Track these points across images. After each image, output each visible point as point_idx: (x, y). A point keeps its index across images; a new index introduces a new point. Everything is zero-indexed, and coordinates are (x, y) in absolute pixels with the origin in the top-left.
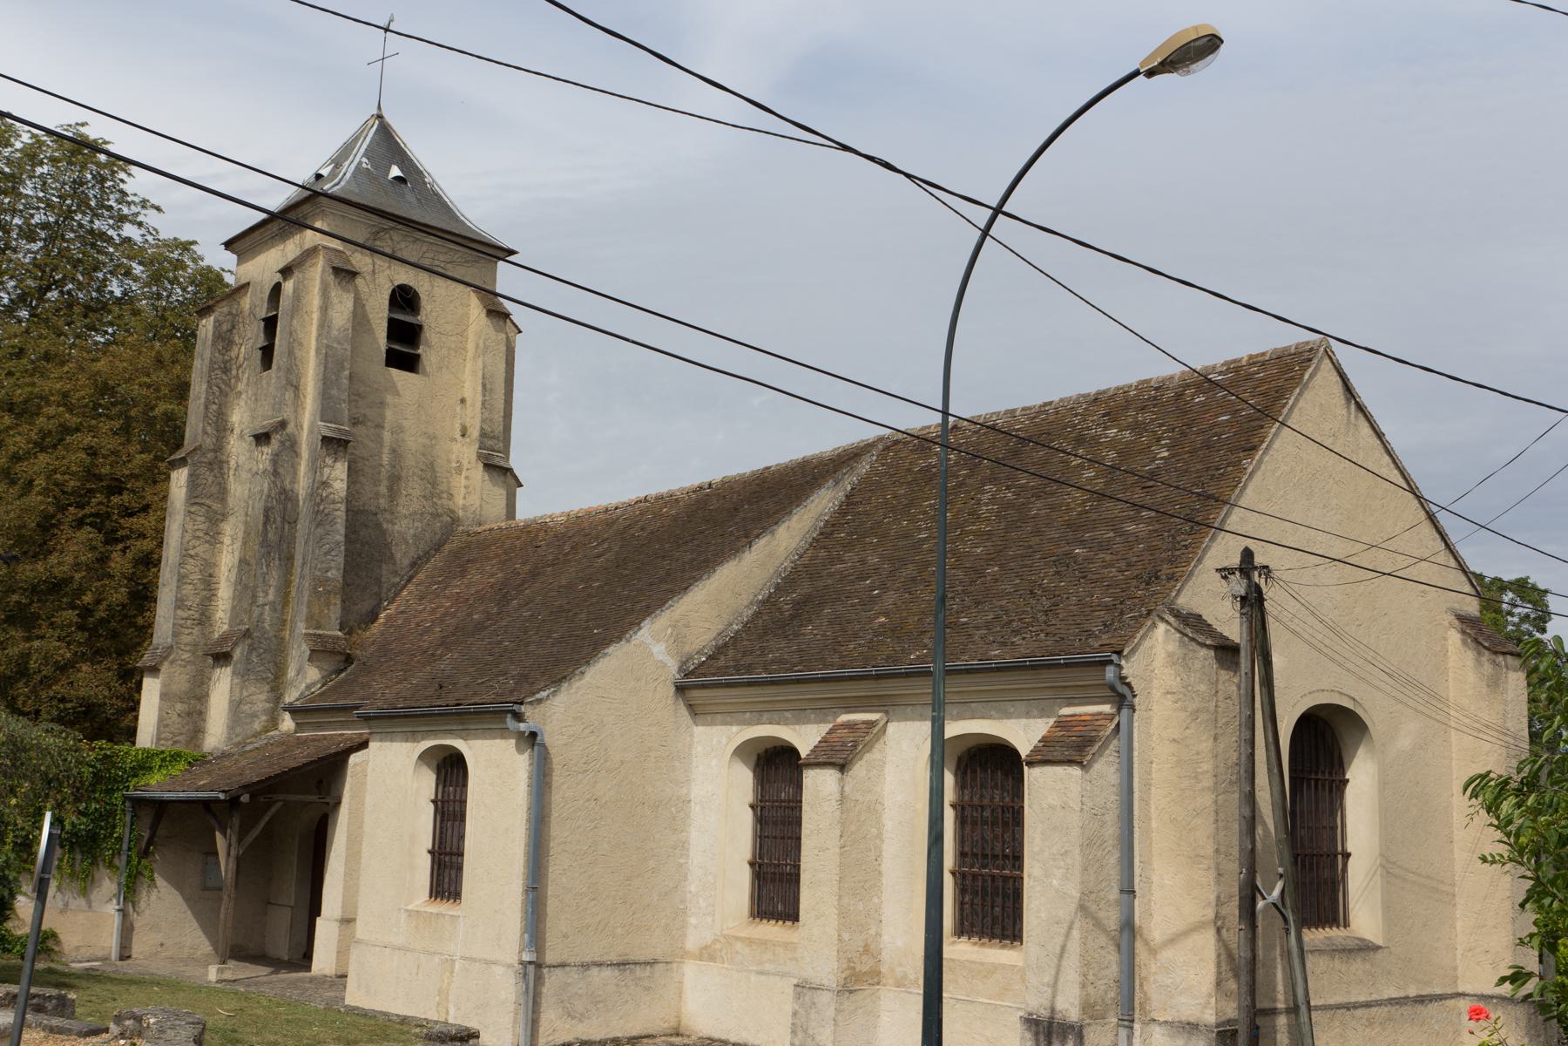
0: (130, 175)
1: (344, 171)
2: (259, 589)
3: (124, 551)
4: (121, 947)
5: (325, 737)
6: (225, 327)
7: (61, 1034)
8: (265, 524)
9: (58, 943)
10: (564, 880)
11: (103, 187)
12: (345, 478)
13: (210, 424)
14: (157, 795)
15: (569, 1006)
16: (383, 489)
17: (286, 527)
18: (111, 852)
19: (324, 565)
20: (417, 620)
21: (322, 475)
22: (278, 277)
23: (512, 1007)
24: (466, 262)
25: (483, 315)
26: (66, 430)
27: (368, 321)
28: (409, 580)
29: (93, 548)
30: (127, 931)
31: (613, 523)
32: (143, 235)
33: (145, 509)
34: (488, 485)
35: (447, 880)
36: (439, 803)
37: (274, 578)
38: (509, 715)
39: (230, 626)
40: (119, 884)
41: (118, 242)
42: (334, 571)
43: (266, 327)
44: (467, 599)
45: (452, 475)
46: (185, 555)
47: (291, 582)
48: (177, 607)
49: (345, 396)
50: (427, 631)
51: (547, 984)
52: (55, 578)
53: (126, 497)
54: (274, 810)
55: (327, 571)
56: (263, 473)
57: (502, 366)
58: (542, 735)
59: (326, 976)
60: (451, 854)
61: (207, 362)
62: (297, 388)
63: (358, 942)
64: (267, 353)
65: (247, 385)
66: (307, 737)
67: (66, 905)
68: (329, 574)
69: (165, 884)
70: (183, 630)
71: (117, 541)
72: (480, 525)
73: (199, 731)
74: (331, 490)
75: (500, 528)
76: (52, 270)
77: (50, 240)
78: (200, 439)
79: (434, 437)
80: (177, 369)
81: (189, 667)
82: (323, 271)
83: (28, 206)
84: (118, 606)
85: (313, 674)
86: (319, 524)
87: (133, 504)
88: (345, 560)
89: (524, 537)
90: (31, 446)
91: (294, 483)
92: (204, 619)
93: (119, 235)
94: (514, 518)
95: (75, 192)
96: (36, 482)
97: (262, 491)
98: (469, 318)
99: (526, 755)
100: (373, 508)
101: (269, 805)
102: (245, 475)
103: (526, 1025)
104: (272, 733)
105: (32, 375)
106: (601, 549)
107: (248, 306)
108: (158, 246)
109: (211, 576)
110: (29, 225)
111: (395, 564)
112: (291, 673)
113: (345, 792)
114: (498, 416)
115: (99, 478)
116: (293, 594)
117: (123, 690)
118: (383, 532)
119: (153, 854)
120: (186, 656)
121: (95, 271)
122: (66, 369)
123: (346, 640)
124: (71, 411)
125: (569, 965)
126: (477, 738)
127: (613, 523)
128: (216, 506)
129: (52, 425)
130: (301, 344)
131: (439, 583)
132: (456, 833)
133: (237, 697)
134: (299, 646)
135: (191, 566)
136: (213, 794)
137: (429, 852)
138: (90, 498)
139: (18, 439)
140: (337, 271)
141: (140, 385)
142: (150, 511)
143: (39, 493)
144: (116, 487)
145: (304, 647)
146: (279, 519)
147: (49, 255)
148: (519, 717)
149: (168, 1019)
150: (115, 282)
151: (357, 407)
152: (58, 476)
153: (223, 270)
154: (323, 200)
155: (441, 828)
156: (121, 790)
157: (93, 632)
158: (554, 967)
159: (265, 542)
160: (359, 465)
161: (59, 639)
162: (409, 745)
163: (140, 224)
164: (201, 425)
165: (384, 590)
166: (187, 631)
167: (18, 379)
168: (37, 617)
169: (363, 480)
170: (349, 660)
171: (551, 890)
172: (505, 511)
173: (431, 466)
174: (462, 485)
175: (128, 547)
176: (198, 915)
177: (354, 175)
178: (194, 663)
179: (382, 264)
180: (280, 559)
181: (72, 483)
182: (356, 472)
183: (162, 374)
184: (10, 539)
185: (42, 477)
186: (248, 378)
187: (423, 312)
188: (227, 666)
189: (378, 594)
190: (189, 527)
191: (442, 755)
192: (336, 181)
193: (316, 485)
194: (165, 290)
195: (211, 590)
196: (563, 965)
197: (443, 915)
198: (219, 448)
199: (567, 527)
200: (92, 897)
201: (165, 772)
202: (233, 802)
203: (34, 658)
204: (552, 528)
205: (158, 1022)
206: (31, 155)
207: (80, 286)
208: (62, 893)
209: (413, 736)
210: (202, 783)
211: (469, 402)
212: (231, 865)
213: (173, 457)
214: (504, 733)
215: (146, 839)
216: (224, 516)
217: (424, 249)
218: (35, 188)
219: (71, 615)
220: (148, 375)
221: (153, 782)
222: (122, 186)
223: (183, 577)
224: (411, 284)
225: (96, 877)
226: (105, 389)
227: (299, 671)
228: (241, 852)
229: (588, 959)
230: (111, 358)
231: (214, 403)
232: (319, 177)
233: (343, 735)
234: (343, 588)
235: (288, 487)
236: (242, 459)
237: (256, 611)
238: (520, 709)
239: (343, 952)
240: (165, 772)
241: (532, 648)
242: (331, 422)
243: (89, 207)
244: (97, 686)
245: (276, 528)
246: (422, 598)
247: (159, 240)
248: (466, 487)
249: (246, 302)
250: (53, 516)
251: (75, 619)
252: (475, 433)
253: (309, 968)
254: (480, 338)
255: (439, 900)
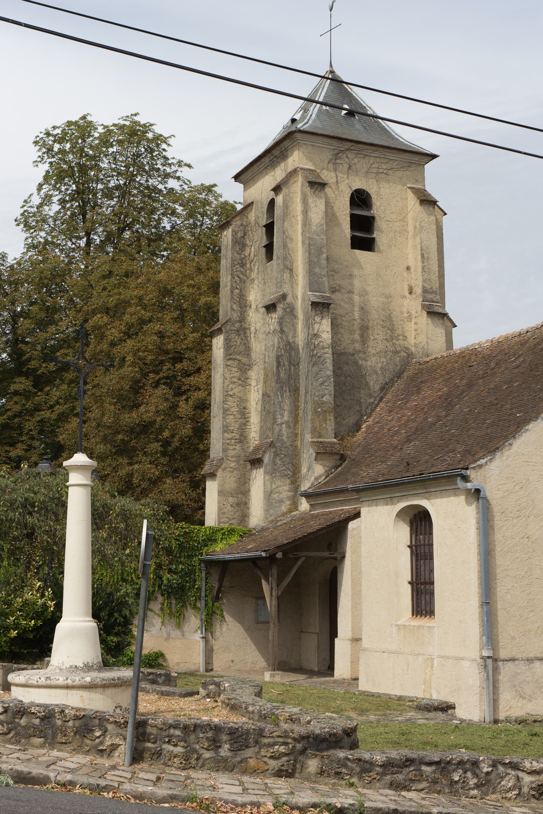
0: (169, 145)
1: (310, 113)
2: (277, 413)
3: (187, 400)
4: (206, 663)
5: (330, 512)
6: (240, 235)
7: (168, 696)
8: (278, 367)
9: (165, 660)
10: (509, 596)
11: (152, 156)
12: (330, 330)
13: (235, 303)
14: (221, 557)
15: (520, 690)
16: (357, 337)
17: (292, 368)
18: (194, 598)
19: (320, 393)
20: (388, 427)
21: (313, 329)
22: (272, 195)
23: (478, 690)
24: (402, 167)
25: (418, 204)
26: (143, 322)
27: (337, 218)
28: (381, 400)
29: (167, 400)
30: (209, 653)
31: (526, 343)
32: (181, 185)
33: (198, 370)
34: (431, 327)
35: (423, 602)
36: (414, 547)
37: (287, 405)
38: (459, 478)
39: (260, 440)
40: (201, 620)
41: (165, 192)
42: (327, 397)
43: (267, 231)
44: (423, 409)
45: (405, 323)
46: (227, 395)
47: (298, 407)
48: (224, 432)
49: (324, 272)
50: (397, 433)
51: (502, 674)
52: (144, 422)
53: (185, 363)
54: (299, 563)
55: (323, 397)
56: (274, 332)
57: (434, 240)
58: (484, 491)
59: (344, 679)
60: (425, 583)
61: (229, 260)
62: (291, 270)
63: (364, 650)
64: (269, 248)
65: (258, 273)
66: (318, 514)
67: (169, 634)
68: (324, 399)
69: (231, 619)
70: (229, 447)
71: (181, 394)
72: (428, 356)
73: (246, 516)
74: (321, 339)
75: (442, 357)
76: (125, 217)
77: (123, 196)
78: (229, 314)
79: (390, 297)
80: (211, 274)
81: (235, 472)
82: (302, 185)
83: (106, 176)
84: (185, 437)
85: (319, 470)
86: (314, 365)
87: (190, 368)
88: (335, 389)
89: (460, 360)
90: (121, 335)
91: (295, 337)
92: (243, 439)
93: (165, 188)
94: (452, 349)
95: (134, 161)
96: (127, 359)
97: (274, 345)
98: (407, 208)
99: (474, 506)
100: (351, 351)
101: (297, 559)
102: (261, 336)
103: (489, 703)
104: (295, 513)
105: (118, 288)
106: (518, 362)
107: (253, 219)
108: (191, 191)
109: (244, 408)
110: (107, 188)
111: (369, 389)
112: (304, 470)
113: (347, 549)
114: (435, 277)
115: (167, 352)
116: (301, 415)
117: (194, 494)
118: (360, 367)
119: (222, 598)
120: (232, 465)
121: (152, 214)
122: (139, 281)
123: (339, 444)
124: (145, 309)
125: (518, 660)
126: (437, 498)
127: (526, 343)
128: (244, 360)
129: (134, 320)
130: (291, 239)
131: (402, 399)
132: (427, 569)
133: (268, 489)
134: (308, 451)
135: (231, 403)
136: (258, 553)
137: (409, 583)
138: (162, 367)
139: (113, 330)
140: (312, 184)
141: (188, 286)
142: (202, 371)
143: (129, 366)
144: (178, 358)
145: (312, 451)
146: (286, 363)
147: (122, 206)
148: (466, 479)
149: (237, 684)
150: (165, 220)
151: (334, 280)
152: (141, 353)
153: (236, 203)
154: (298, 136)
155: (416, 565)
156: (198, 556)
157: (172, 457)
158: (506, 660)
159: (278, 380)
160: (339, 320)
161: (150, 463)
162: (389, 508)
163: (178, 178)
164: (229, 305)
165: (364, 408)
166: (232, 448)
167: (109, 291)
168: (134, 449)
169: (343, 331)
170: (343, 458)
171: (500, 605)
172: (445, 344)
173: (389, 317)
174: (413, 329)
175: (189, 397)
176: (255, 641)
177: (318, 116)
178: (238, 469)
179: (342, 176)
180: (290, 391)
181: (150, 358)
182: (337, 326)
183: (201, 277)
184: (113, 398)
185: (131, 354)
186: (258, 269)
187: (374, 207)
188: (260, 468)
189: (359, 411)
190: (228, 376)
191: (412, 513)
192: (306, 121)
193: (310, 337)
194: (199, 221)
195: (245, 418)
196: (513, 660)
197: (423, 627)
198: (242, 319)
199: (491, 350)
200: (185, 629)
201: (225, 542)
202: (272, 558)
203: (136, 476)
204: (480, 352)
205: (230, 685)
206: (105, 140)
207: (144, 226)
208: (165, 627)
209: (391, 501)
210: (250, 547)
211: (412, 269)
212: (274, 602)
213: (213, 329)
214: (456, 491)
215: (216, 589)
216: (250, 366)
217: (372, 162)
218: (109, 162)
219: (156, 446)
220: (193, 279)
221: (218, 549)
222: (164, 153)
223: (227, 410)
224: (364, 188)
225: (186, 616)
226: (166, 292)
227: (309, 469)
228: (280, 593)
229: (531, 655)
230: (168, 270)
231: (237, 288)
232: (293, 121)
233: (343, 510)
234: (334, 408)
235: (291, 340)
236: (259, 325)
237: (277, 429)
238: (466, 473)
239: (355, 662)
240: (225, 542)
241: (472, 431)
242: (316, 292)
243: (144, 170)
244: (177, 493)
245: (285, 370)
246: (390, 411)
247: (191, 187)
248: (416, 330)
249: (252, 216)
250: (139, 381)
251: (159, 449)
252: (419, 290)
253: (332, 675)
254: (416, 221)
255: (419, 617)
